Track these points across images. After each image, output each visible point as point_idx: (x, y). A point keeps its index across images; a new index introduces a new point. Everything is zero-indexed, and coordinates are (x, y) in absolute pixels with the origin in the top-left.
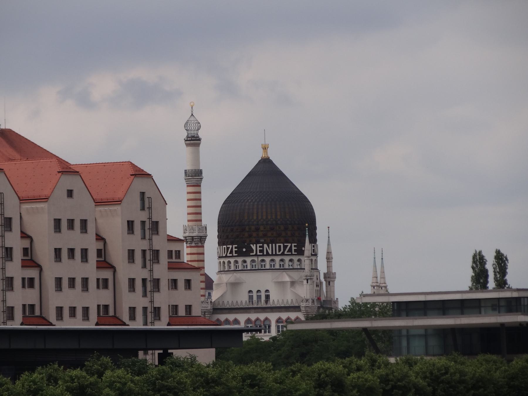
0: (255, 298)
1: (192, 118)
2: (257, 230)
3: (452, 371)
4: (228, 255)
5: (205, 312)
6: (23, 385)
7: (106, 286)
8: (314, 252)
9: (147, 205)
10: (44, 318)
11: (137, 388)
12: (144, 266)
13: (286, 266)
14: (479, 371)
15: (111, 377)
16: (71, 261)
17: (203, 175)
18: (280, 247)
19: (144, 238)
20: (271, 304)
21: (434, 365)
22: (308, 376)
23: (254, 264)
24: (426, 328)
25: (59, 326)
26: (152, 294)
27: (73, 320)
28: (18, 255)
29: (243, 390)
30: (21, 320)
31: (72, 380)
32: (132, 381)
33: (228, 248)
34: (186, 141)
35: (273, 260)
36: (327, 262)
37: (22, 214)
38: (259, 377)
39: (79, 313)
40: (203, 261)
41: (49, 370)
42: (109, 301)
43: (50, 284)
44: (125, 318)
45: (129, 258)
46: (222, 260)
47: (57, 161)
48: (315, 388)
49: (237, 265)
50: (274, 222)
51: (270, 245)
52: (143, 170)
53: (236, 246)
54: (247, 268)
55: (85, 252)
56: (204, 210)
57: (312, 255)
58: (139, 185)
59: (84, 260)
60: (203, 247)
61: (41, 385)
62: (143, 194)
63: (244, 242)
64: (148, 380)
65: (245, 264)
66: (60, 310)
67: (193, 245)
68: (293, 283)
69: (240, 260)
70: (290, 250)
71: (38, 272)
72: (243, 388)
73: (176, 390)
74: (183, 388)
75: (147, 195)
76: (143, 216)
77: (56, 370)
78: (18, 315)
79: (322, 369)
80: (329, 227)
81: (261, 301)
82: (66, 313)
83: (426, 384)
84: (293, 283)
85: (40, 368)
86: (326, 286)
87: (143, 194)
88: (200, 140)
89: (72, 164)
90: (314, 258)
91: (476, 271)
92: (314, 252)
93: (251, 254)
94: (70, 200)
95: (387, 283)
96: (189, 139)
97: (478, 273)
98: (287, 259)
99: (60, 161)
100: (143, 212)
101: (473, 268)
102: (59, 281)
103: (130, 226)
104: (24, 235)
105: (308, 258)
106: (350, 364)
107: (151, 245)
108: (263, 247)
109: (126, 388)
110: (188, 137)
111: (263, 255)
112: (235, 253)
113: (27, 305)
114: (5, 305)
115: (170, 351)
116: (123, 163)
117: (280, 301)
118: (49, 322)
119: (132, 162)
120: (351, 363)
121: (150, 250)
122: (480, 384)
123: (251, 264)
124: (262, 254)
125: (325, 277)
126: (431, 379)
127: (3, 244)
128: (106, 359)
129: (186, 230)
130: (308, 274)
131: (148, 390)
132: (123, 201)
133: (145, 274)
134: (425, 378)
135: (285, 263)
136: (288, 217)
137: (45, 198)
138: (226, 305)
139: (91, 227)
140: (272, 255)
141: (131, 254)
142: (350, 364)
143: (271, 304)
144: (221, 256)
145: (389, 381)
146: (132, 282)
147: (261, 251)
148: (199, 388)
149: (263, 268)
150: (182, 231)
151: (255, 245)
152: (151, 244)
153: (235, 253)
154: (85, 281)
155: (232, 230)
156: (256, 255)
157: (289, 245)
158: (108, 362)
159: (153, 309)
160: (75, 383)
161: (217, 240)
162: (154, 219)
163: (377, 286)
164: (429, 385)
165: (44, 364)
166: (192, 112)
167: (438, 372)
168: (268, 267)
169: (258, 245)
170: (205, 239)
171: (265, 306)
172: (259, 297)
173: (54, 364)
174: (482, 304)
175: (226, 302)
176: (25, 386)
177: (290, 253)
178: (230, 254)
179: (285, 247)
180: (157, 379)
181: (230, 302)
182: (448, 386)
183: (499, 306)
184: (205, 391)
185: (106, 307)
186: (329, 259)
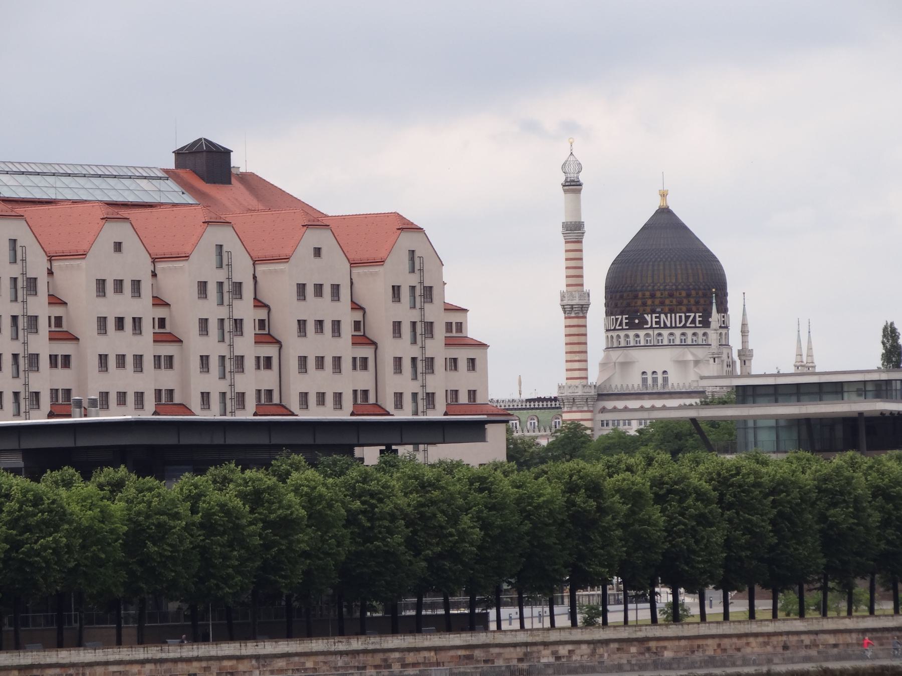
0: (650, 381)
1: (572, 158)
2: (653, 296)
3: (744, 471)
4: (617, 328)
5: (587, 399)
6: (182, 489)
7: (365, 366)
8: (724, 324)
9: (417, 267)
10: (380, 406)
11: (331, 493)
12: (414, 342)
13: (689, 342)
14: (781, 471)
15: (297, 479)
16: (319, 336)
17: (586, 228)
18: (680, 317)
19: (413, 307)
20: (670, 388)
21: (722, 464)
22: (557, 478)
23: (648, 339)
24: (777, 418)
25: (201, 415)
26: (424, 376)
27: (321, 408)
28: (250, 329)
29: (469, 495)
30: (444, 409)
31: (246, 483)
32: (324, 485)
33: (617, 319)
34: (564, 186)
35: (671, 334)
36: (742, 336)
37: (353, 280)
38: (491, 479)
39: (329, 399)
40: (585, 335)
41: (223, 471)
42: (370, 386)
43: (292, 364)
44: (389, 405)
45: (394, 332)
46: (610, 334)
47: (302, 211)
48: (564, 492)
49: (628, 340)
50: (674, 287)
51: (669, 315)
52: (412, 223)
53: (627, 316)
54: (640, 343)
55: (337, 325)
56: (586, 272)
57: (721, 327)
58: (407, 241)
59: (336, 334)
60: (585, 317)
61: (204, 489)
62: (412, 252)
63: (637, 311)
64: (346, 483)
65: (638, 339)
66: (304, 396)
67: (573, 315)
68: (697, 362)
69: (631, 333)
70: (694, 321)
71: (278, 348)
72: (469, 493)
73: (381, 496)
74: (390, 493)
75: (417, 254)
76: (413, 280)
77: (232, 471)
78: (251, 403)
79: (575, 469)
80: (744, 293)
81: (657, 385)
82: (312, 399)
83: (711, 487)
84: (697, 362)
85: (213, 468)
86: (741, 367)
87: (412, 252)
88: (580, 185)
89: (330, 215)
90: (724, 331)
91: (887, 347)
92: (724, 324)
93: (645, 326)
94: (318, 260)
95: (815, 361)
96: (567, 184)
97: (890, 350)
98: (689, 332)
99: (306, 209)
100: (412, 275)
101: (883, 343)
102: (303, 360)
103: (396, 291)
104: (259, 304)
105: (715, 332)
106: (619, 463)
107: (423, 316)
108: (659, 317)
109: (315, 494)
110: (566, 181)
111: (660, 328)
112: (626, 326)
113: (263, 391)
114: (27, 390)
115: (394, 447)
116: (389, 215)
117: (681, 385)
118: (290, 411)
119: (400, 213)
120: (620, 461)
121: (23, 315)
122: (782, 487)
123: (645, 339)
124: (658, 326)
125: (739, 355)
126: (718, 482)
127: (231, 315)
128: (298, 458)
129: (564, 297)
130: (716, 351)
131: (345, 496)
132: (191, 257)
133: (415, 352)
134: (710, 481)
135: (687, 338)
136: (691, 280)
137: (62, 254)
138: (614, 389)
139: (345, 293)
140: (671, 327)
141: (397, 326)
142: (619, 463)
145: (663, 483)
146: (398, 361)
147: (657, 323)
148: (412, 493)
149: (660, 344)
150: (559, 298)
151: (650, 315)
152: (423, 316)
153: (626, 326)
154: (337, 361)
155: (621, 297)
156: (651, 328)
157: (692, 315)
158: (300, 461)
159: (425, 395)
160: (249, 486)
161: (603, 309)
162: (427, 284)
163: (802, 366)
164: (714, 490)
165: (218, 463)
166: (571, 150)
167: (727, 472)
168: (666, 342)
169: (654, 315)
170: (588, 308)
172: (655, 380)
173: (230, 463)
174: (845, 389)
175: (613, 386)
176: (184, 490)
177: (693, 325)
178: (619, 326)
179: (687, 318)
180: (358, 482)
181: (619, 386)
182: (739, 490)
183: (865, 391)
184: (420, 496)
185: (365, 393)
186: (744, 332)
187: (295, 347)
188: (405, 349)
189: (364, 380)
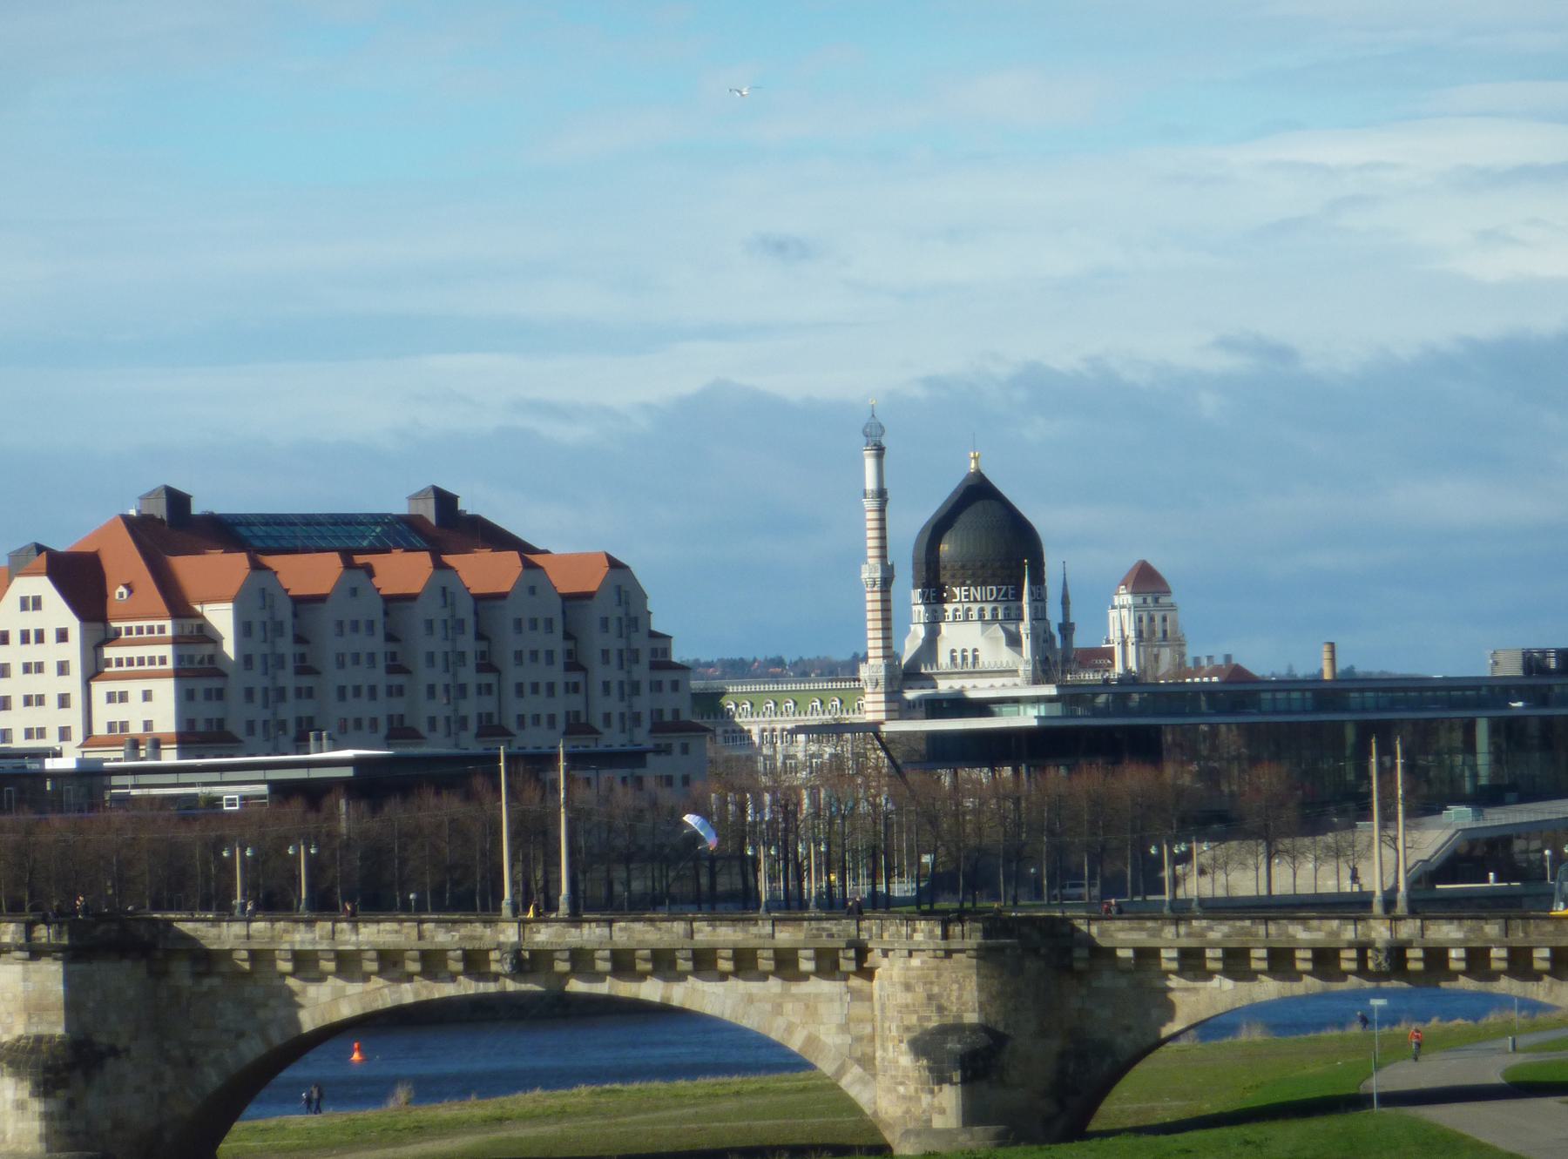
18: (992, 590)
51: (979, 588)
55: (550, 655)
70: (1006, 595)
80: (1064, 562)
93: (954, 600)
108: (968, 590)
111: (970, 602)
140: (982, 601)
143: (979, 668)
144: (981, 589)
147: (966, 597)
154: (551, 687)
156: (960, 602)
157: (1005, 587)
169: (963, 588)
171: (972, 670)
172: (964, 658)
179: (999, 591)
187: (513, 674)
188: (614, 675)
189: (576, 702)
